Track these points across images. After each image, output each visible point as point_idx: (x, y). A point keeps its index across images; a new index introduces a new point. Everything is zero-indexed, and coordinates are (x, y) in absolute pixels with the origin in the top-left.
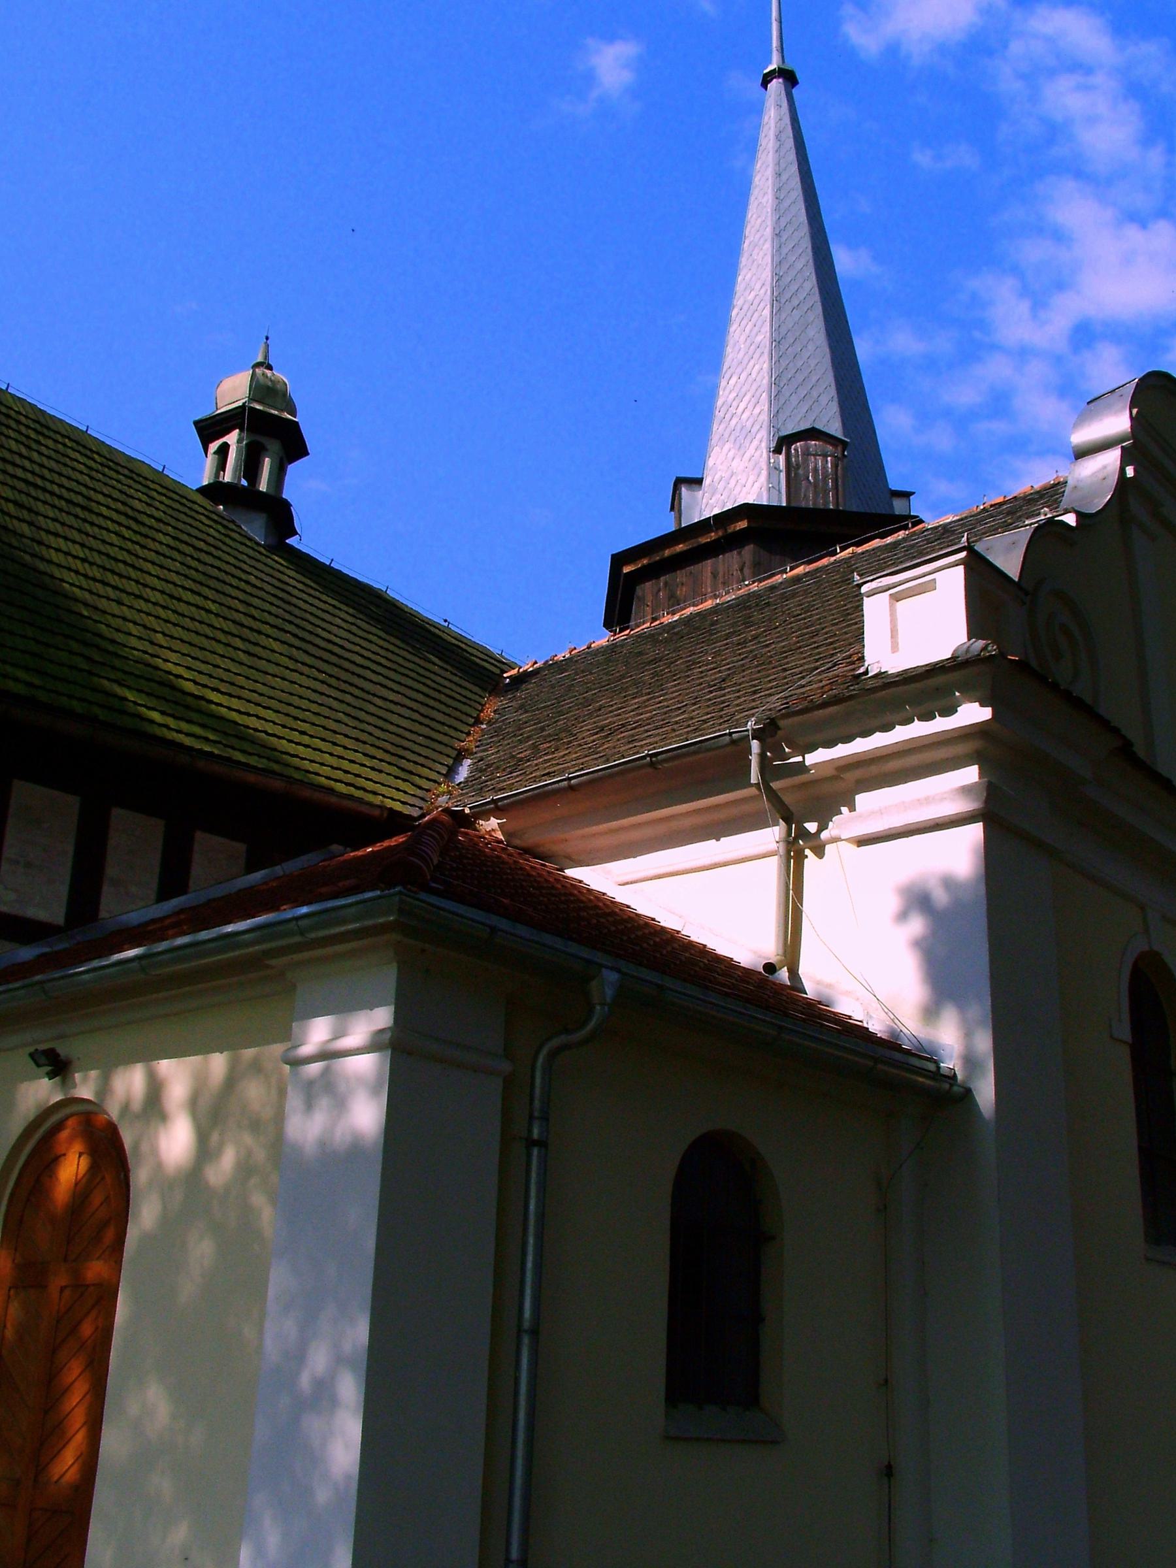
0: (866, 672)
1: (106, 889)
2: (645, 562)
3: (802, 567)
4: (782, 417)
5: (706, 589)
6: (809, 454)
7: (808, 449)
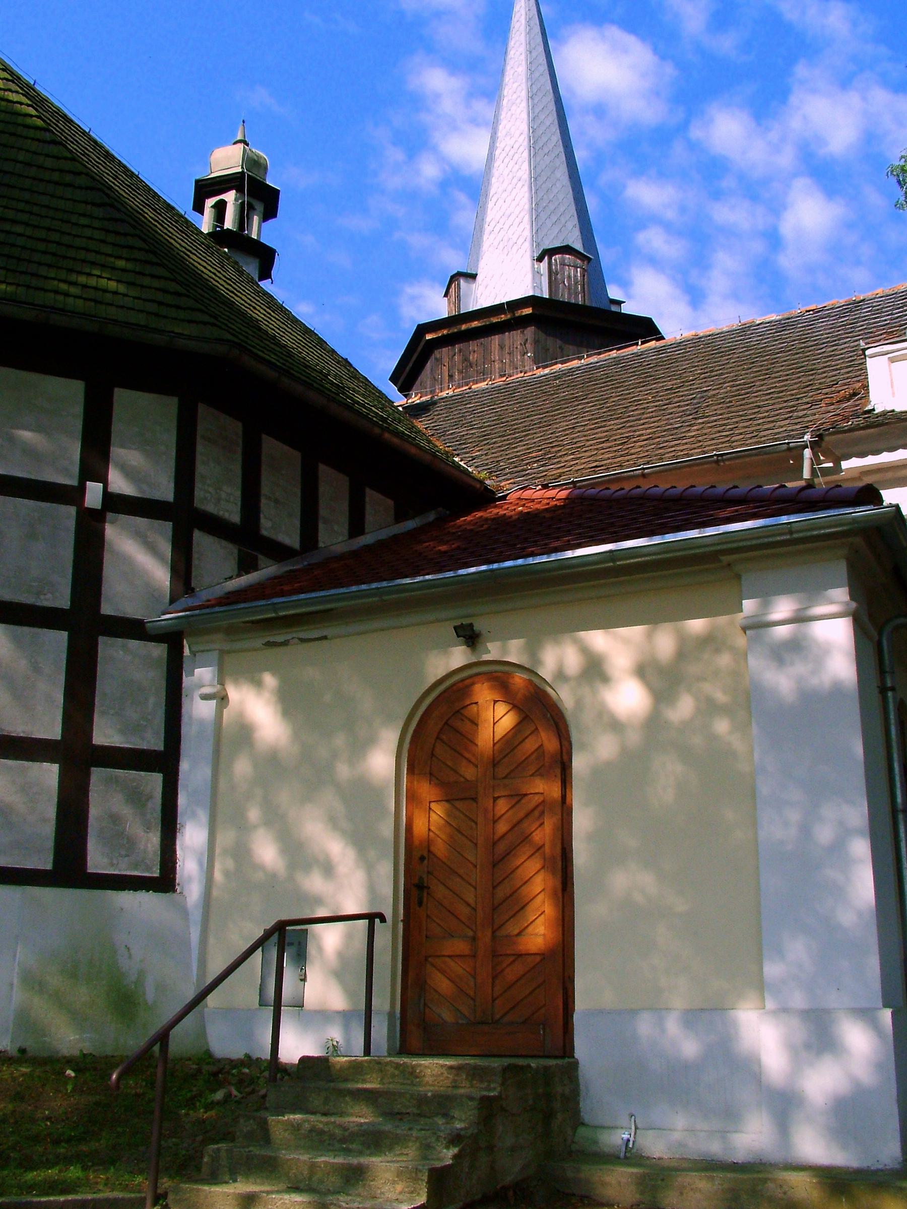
0: (874, 410)
1: (321, 526)
2: (445, 332)
4: (541, 235)
5: (495, 358)
6: (565, 265)
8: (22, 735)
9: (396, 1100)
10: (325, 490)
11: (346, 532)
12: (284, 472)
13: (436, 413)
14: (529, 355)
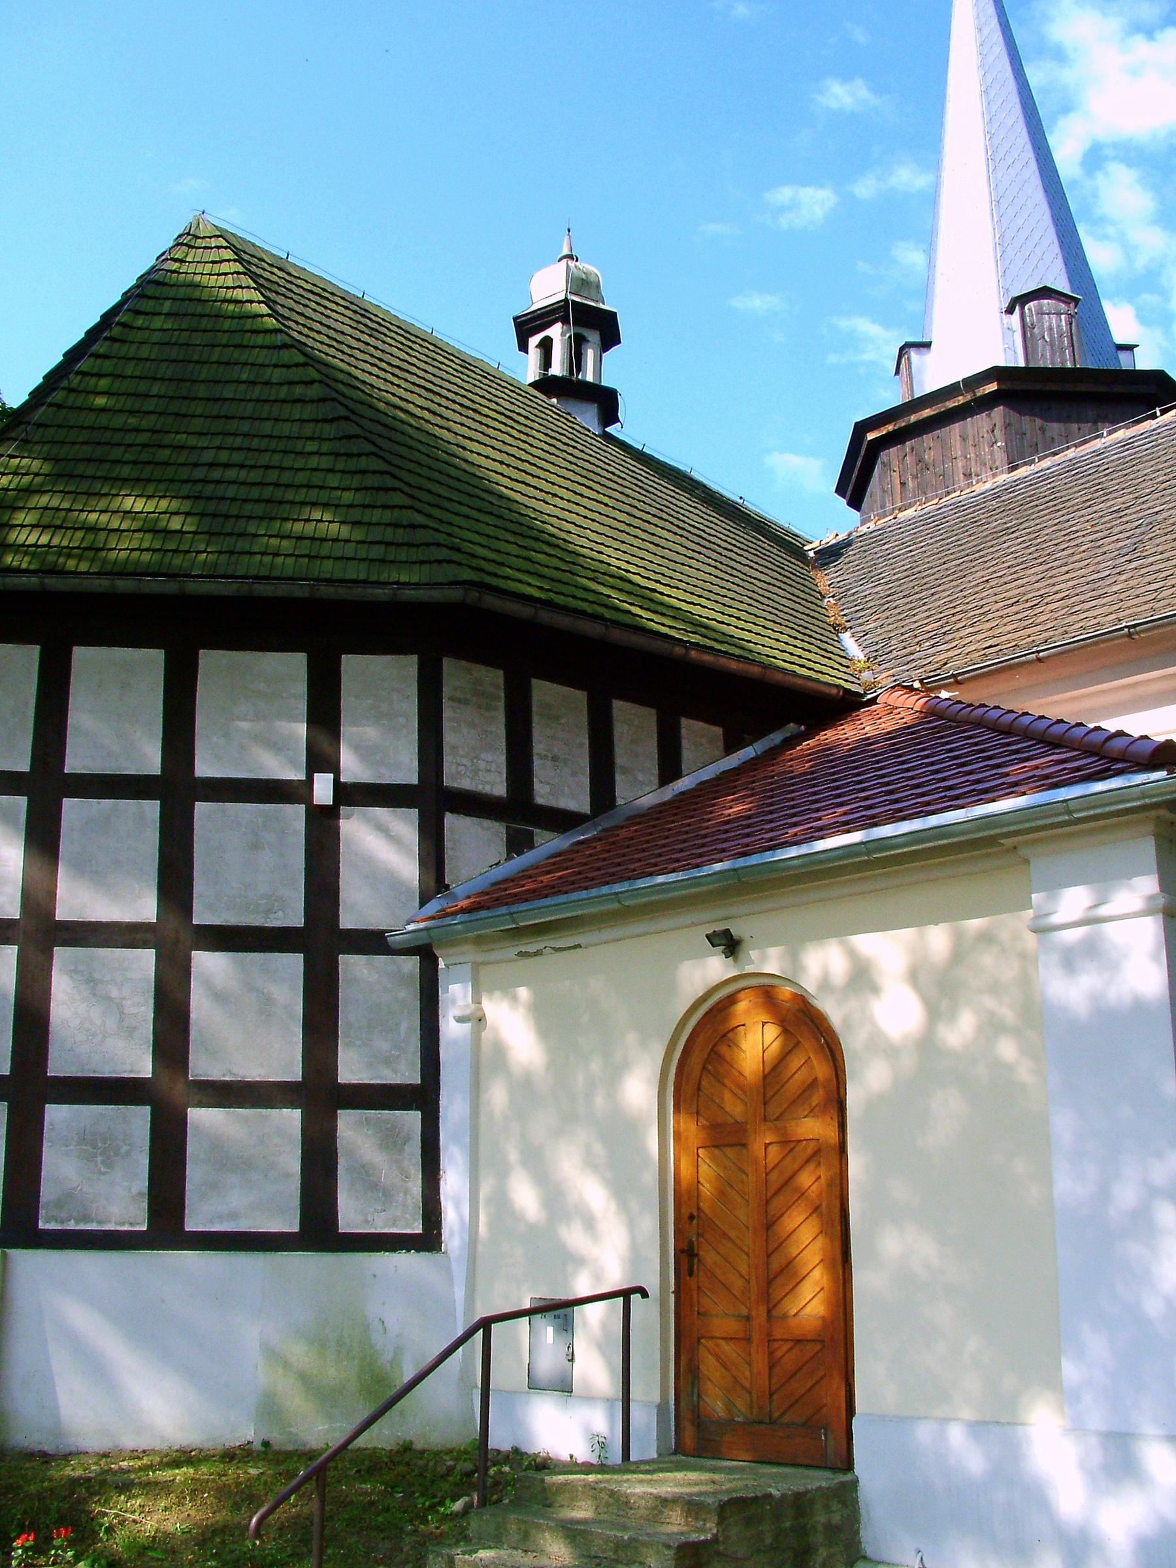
1: (619, 778)
3: (1122, 431)
5: (956, 453)
7: (1041, 308)
8: (258, 1079)
9: (593, 1541)
10: (621, 731)
11: (656, 781)
12: (563, 721)
13: (847, 560)
14: (999, 444)
